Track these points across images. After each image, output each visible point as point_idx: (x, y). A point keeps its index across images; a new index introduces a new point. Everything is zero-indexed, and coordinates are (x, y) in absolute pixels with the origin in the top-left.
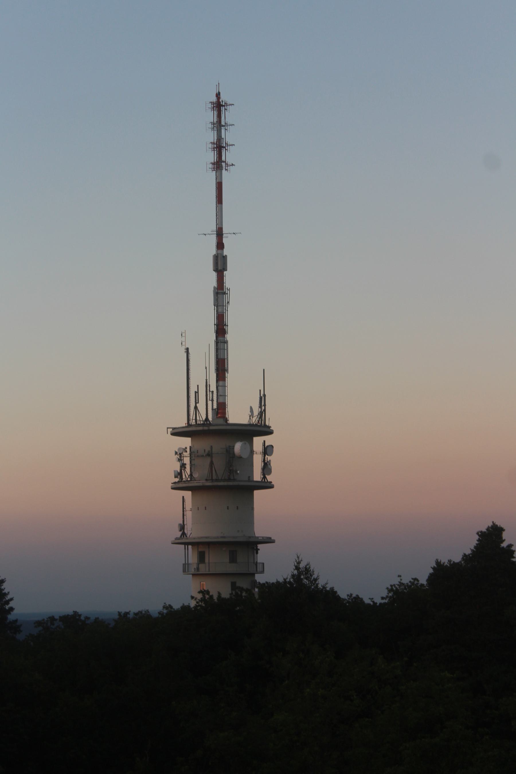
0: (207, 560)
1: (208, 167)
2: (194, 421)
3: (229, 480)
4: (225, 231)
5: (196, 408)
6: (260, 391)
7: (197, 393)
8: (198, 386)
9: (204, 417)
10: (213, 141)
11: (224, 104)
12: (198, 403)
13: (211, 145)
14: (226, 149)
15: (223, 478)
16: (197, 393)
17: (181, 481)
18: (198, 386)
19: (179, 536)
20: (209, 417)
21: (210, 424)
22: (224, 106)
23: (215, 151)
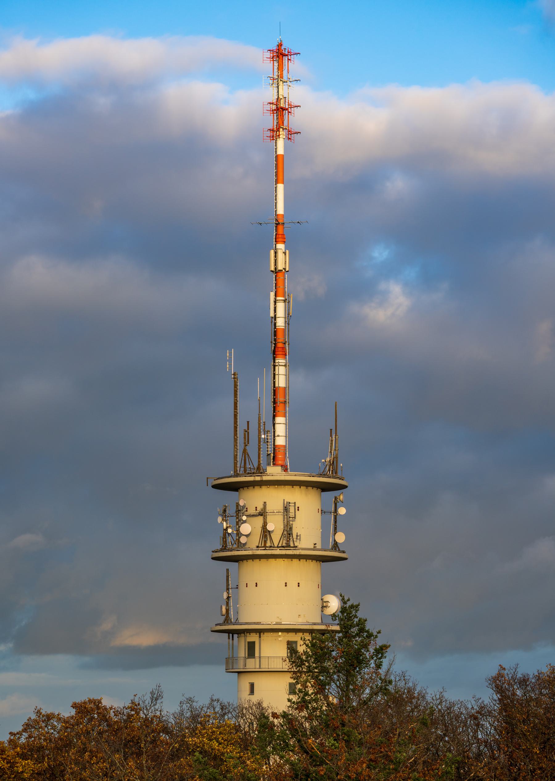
0: (257, 654)
1: (265, 56)
2: (242, 469)
3: (288, 546)
4: (277, 316)
5: (245, 451)
6: (331, 430)
7: (247, 432)
8: (248, 422)
9: (256, 465)
10: (272, 128)
11: (286, 53)
12: (248, 443)
13: (269, 132)
14: (289, 112)
15: (280, 545)
16: (247, 432)
17: (225, 549)
18: (248, 422)
19: (221, 622)
20: (298, 528)
21: (286, 363)
22: (287, 55)
23: (275, 115)
